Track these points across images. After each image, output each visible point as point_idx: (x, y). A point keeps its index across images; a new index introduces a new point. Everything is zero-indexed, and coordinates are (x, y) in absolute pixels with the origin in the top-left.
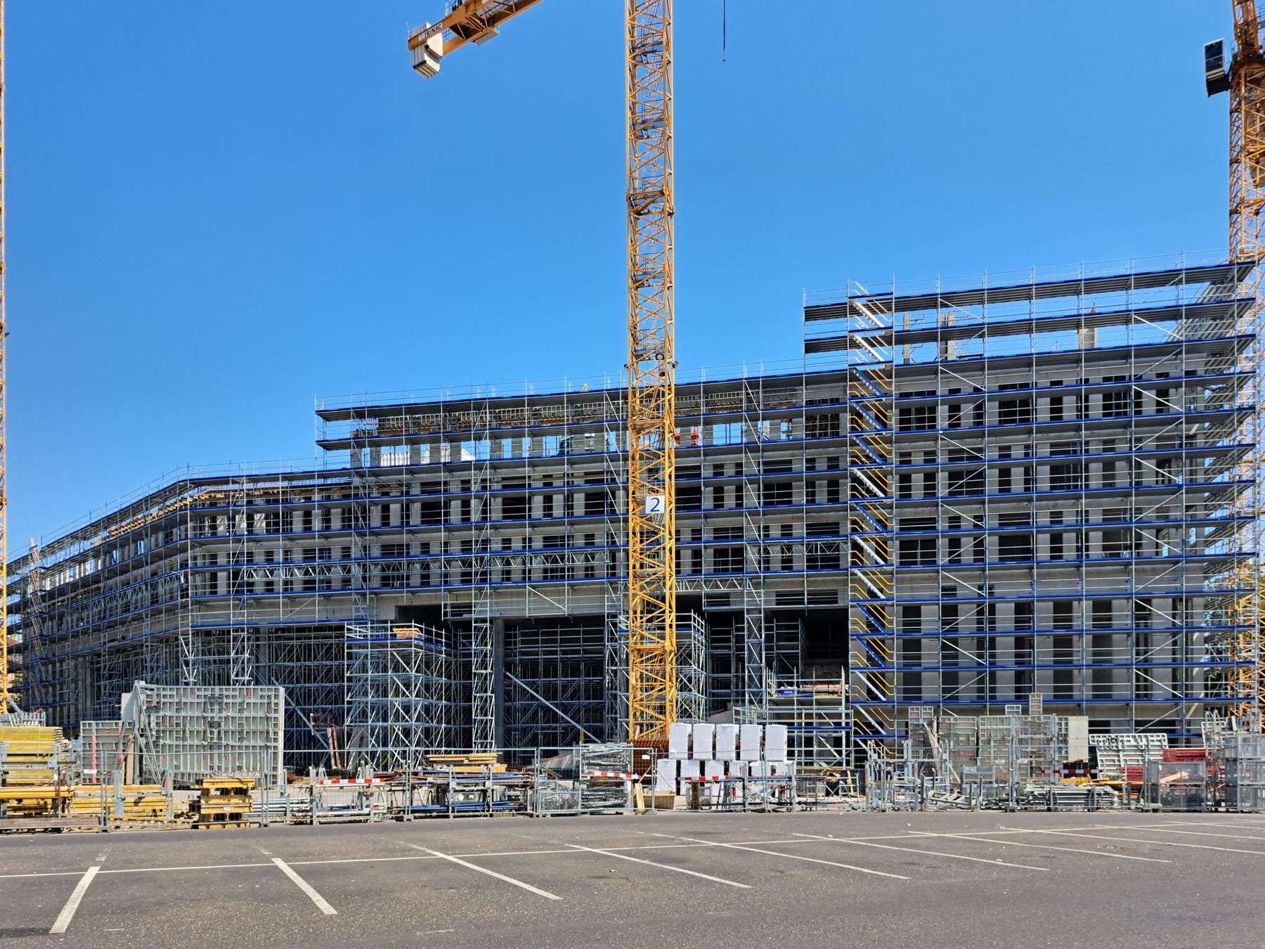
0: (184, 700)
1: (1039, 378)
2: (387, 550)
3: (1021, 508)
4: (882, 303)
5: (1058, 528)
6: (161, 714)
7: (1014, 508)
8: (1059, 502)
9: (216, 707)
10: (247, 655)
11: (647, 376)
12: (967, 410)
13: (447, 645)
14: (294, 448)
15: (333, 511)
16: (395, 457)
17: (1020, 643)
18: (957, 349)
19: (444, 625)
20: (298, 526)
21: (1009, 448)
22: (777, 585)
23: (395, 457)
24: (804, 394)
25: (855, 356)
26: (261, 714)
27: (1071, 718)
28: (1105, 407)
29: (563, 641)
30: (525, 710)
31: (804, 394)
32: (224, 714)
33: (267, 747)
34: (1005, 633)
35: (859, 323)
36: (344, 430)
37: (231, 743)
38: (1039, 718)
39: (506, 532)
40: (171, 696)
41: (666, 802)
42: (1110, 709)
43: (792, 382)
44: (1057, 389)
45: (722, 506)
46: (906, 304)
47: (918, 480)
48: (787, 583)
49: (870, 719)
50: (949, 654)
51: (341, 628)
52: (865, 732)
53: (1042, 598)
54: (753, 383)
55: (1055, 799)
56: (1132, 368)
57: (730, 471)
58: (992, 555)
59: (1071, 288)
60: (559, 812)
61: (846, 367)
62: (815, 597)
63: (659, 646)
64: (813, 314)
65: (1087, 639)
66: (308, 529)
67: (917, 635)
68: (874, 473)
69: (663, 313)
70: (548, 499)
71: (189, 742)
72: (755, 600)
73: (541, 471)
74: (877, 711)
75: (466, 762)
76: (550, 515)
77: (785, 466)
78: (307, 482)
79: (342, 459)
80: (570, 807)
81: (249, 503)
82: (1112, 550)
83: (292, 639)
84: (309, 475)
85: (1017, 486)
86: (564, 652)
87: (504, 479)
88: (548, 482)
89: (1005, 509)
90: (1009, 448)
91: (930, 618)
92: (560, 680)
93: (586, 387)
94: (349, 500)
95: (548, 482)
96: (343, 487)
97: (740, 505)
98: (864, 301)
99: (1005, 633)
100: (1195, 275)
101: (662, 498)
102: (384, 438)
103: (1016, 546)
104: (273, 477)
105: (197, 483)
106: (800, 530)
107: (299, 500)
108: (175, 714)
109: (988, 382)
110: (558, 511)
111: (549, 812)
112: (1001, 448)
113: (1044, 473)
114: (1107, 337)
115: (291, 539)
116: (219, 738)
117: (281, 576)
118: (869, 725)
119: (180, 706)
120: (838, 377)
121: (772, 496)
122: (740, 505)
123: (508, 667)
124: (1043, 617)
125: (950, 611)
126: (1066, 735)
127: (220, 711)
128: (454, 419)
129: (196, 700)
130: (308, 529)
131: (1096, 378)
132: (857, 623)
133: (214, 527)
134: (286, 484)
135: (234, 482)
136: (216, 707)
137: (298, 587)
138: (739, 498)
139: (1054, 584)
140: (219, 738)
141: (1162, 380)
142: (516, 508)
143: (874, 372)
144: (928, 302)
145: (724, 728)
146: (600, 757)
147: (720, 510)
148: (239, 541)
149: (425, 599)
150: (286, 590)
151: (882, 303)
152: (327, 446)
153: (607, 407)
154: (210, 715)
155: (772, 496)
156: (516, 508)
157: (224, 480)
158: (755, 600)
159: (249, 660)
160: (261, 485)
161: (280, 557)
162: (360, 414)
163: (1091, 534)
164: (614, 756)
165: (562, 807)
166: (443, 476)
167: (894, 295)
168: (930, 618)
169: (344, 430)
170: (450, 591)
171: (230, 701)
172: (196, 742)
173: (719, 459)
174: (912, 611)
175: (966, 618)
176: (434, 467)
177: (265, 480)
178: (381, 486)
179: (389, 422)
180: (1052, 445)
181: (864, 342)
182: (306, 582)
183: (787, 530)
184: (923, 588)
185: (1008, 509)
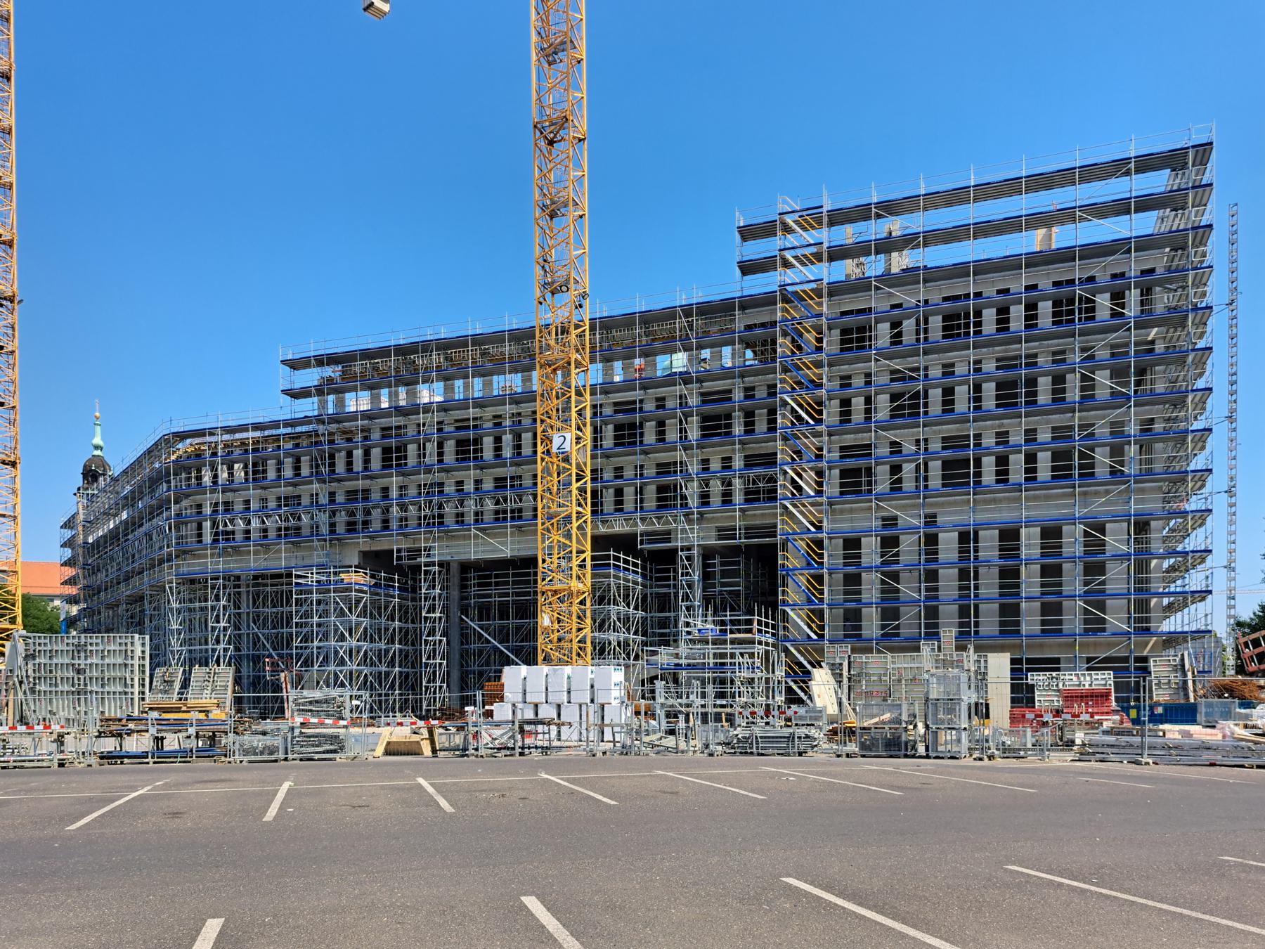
0: (55, 648)
1: (877, 302)
2: (352, 495)
3: (862, 438)
4: (812, 218)
5: (896, 459)
6: (37, 661)
7: (958, 430)
8: (1005, 421)
9: (82, 654)
10: (438, 591)
11: (560, 311)
12: (1017, 313)
13: (644, 576)
14: (258, 396)
15: (302, 458)
16: (358, 402)
17: (964, 575)
18: (901, 261)
19: (399, 570)
20: (340, 468)
21: (953, 365)
22: (717, 519)
23: (358, 402)
24: (740, 321)
25: (790, 276)
26: (120, 660)
27: (989, 655)
28: (1055, 314)
29: (515, 583)
30: (481, 652)
31: (740, 321)
32: (89, 661)
33: (126, 693)
34: (949, 565)
35: (791, 240)
36: (311, 377)
37: (95, 688)
38: (951, 655)
39: (617, 461)
40: (97, 644)
41: (415, 748)
42: (1060, 645)
43: (725, 308)
44: (897, 312)
45: (849, 421)
46: (838, 218)
47: (858, 403)
48: (721, 516)
49: (802, 659)
50: (889, 591)
51: (289, 575)
52: (795, 672)
53: (1030, 523)
54: (687, 311)
55: (757, 743)
56: (1077, 271)
57: (761, 393)
58: (935, 482)
59: (1011, 187)
60: (259, 758)
61: (776, 288)
62: (751, 532)
63: (566, 586)
64: (748, 233)
65: (876, 576)
66: (350, 470)
67: (1100, 558)
68: (804, 399)
69: (576, 250)
70: (498, 440)
71: (60, 688)
72: (692, 536)
73: (490, 412)
74: (806, 650)
75: (184, 709)
76: (663, 440)
77: (726, 396)
78: (274, 432)
79: (308, 407)
80: (271, 753)
81: (440, 430)
82: (1061, 472)
83: (266, 585)
84: (275, 424)
85: (858, 416)
86: (518, 594)
87: (457, 421)
88: (498, 421)
89: (948, 431)
90: (953, 365)
91: (871, 551)
92: (513, 622)
93: (618, 311)
94: (318, 446)
95: (498, 421)
96: (308, 434)
97: (868, 419)
98: (796, 216)
99: (949, 565)
100: (1146, 164)
101: (568, 436)
102: (657, 345)
103: (958, 472)
104: (243, 428)
105: (182, 436)
106: (738, 463)
107: (339, 440)
108: (48, 661)
109: (1045, 280)
110: (507, 452)
111: (246, 759)
112: (944, 366)
113: (883, 401)
114: (1062, 237)
115: (482, 469)
116: (86, 685)
117: (471, 506)
118: (800, 665)
119: (52, 654)
120: (767, 300)
121: (623, 437)
122: (868, 419)
123: (464, 610)
124: (989, 543)
125: (890, 543)
126: (985, 674)
127: (86, 658)
128: (403, 363)
129: (66, 648)
130: (350, 470)
131: (936, 298)
132: (791, 560)
133: (199, 478)
134: (257, 434)
135: (211, 434)
136: (82, 654)
137: (488, 517)
138: (279, 470)
139: (1000, 510)
140: (86, 685)
141: (1002, 297)
142: (467, 449)
143: (804, 291)
144: (862, 213)
145: (555, 671)
146: (311, 703)
147: (847, 426)
148: (430, 472)
149: (382, 544)
150: (477, 521)
151: (812, 218)
152: (295, 394)
153: (471, 353)
154: (76, 662)
155: (623, 437)
156: (467, 449)
157: (200, 433)
158: (692, 536)
159: (440, 595)
160: (238, 436)
161: (469, 487)
162: (320, 361)
163: (930, 464)
164: (326, 701)
165: (262, 753)
166: (637, 394)
167: (825, 209)
168: (871, 551)
169: (311, 377)
170: (405, 535)
171: (94, 648)
172: (66, 688)
173: (661, 391)
174: (852, 544)
175: (909, 547)
176: (627, 386)
177: (301, 424)
178: (345, 433)
179: (352, 368)
180: (998, 360)
181: (794, 262)
182: (497, 512)
183: (727, 463)
184: (864, 519)
185: (952, 430)
